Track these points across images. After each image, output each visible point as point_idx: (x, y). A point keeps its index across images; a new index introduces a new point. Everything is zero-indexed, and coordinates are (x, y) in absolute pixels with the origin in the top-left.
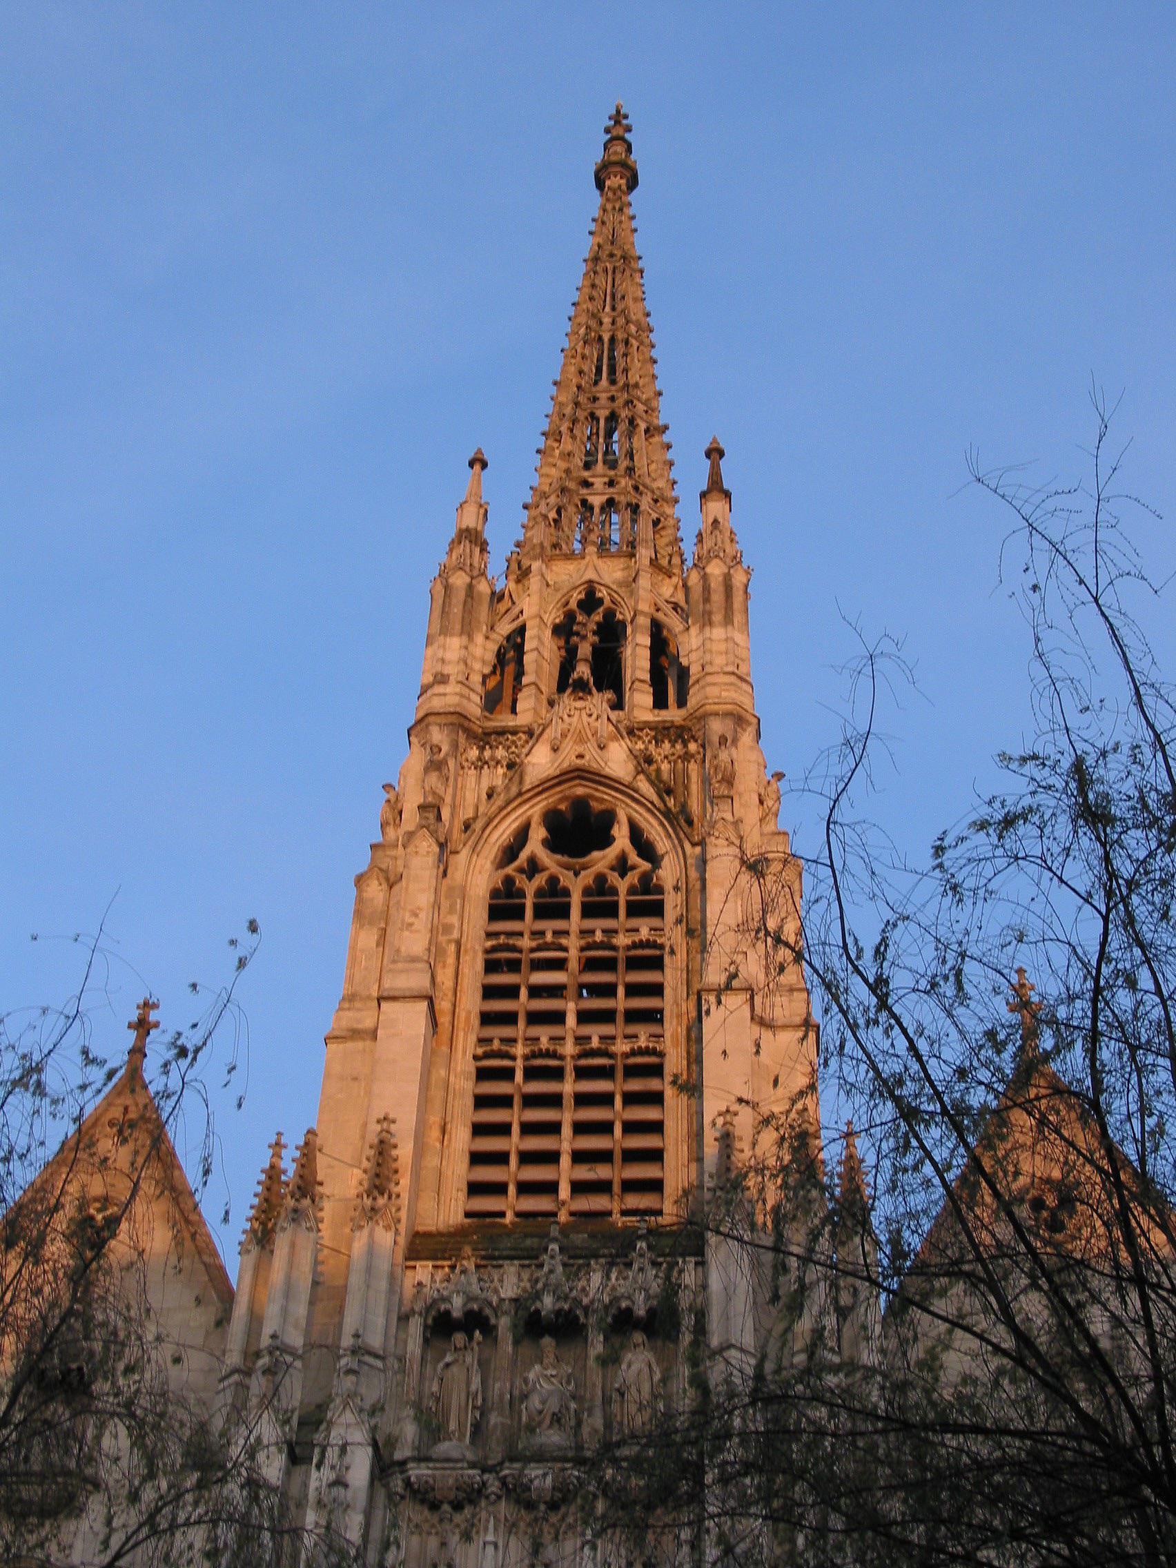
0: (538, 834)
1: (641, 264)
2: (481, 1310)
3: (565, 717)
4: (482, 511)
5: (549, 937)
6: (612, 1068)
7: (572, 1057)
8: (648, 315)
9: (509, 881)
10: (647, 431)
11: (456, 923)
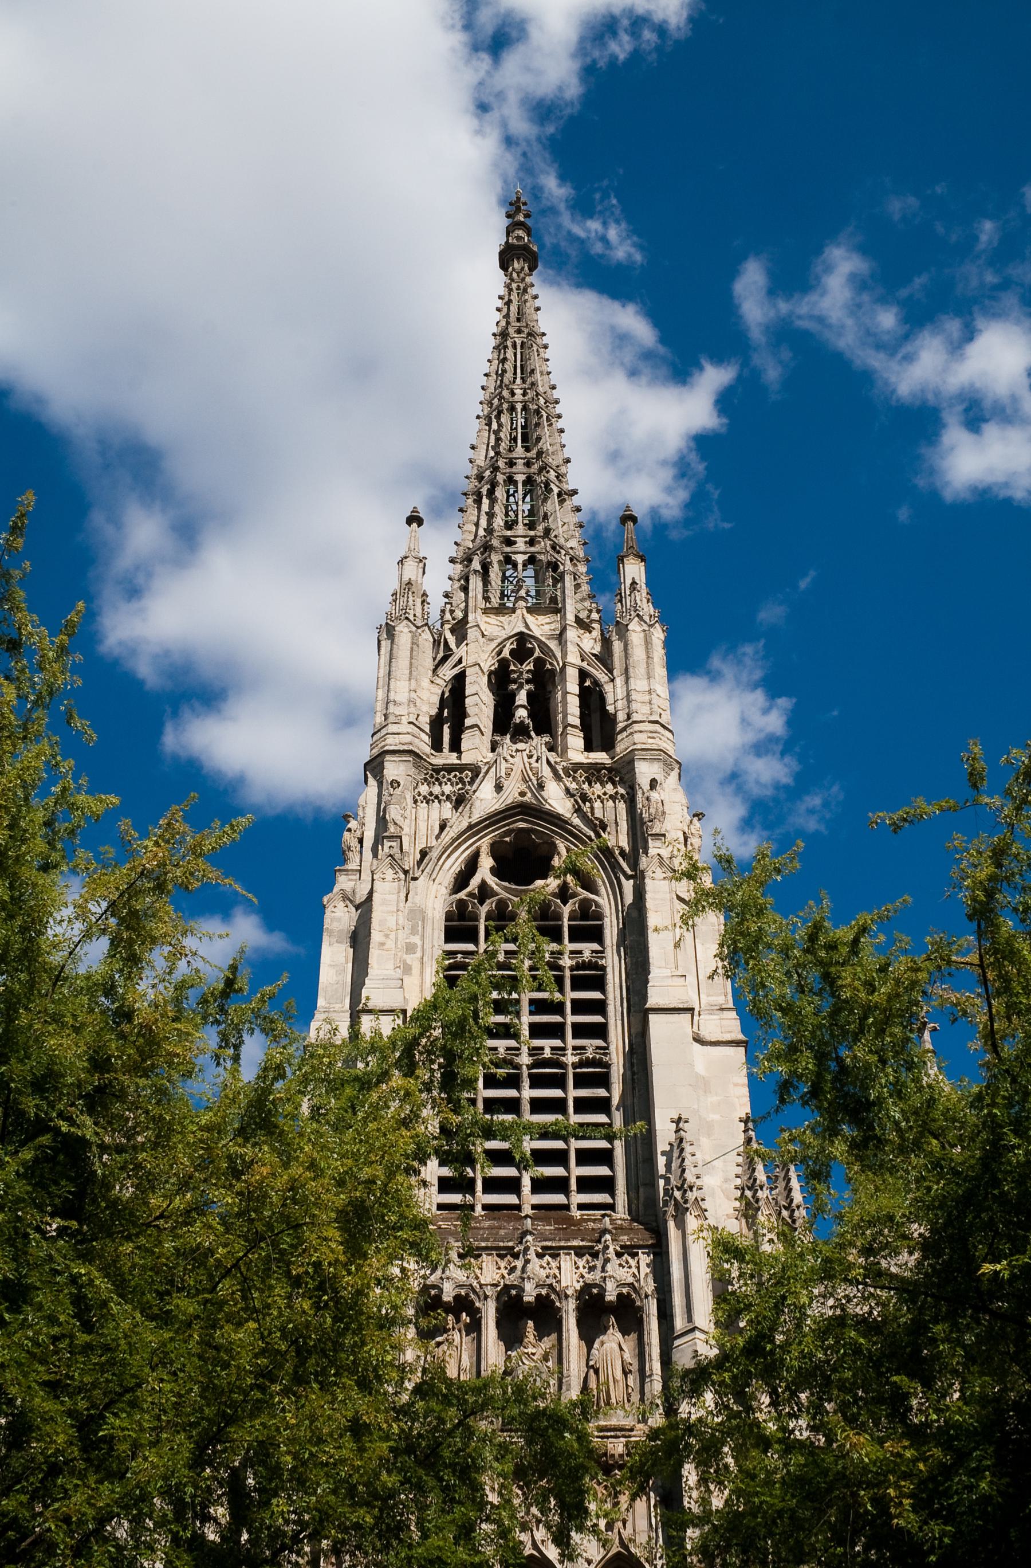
0: (486, 862)
1: (545, 340)
2: (467, 1295)
3: (509, 757)
4: (421, 565)
5: (501, 957)
6: (564, 1076)
7: (527, 1066)
8: (553, 387)
9: (461, 903)
10: (559, 495)
11: (419, 943)
